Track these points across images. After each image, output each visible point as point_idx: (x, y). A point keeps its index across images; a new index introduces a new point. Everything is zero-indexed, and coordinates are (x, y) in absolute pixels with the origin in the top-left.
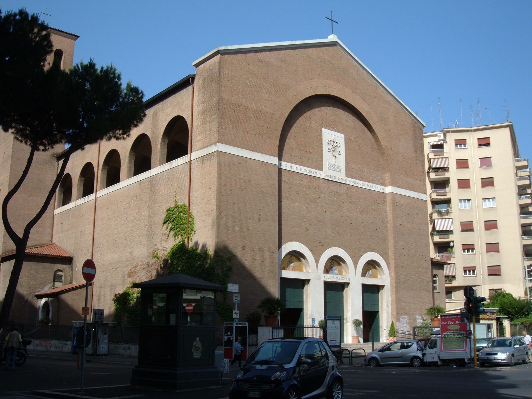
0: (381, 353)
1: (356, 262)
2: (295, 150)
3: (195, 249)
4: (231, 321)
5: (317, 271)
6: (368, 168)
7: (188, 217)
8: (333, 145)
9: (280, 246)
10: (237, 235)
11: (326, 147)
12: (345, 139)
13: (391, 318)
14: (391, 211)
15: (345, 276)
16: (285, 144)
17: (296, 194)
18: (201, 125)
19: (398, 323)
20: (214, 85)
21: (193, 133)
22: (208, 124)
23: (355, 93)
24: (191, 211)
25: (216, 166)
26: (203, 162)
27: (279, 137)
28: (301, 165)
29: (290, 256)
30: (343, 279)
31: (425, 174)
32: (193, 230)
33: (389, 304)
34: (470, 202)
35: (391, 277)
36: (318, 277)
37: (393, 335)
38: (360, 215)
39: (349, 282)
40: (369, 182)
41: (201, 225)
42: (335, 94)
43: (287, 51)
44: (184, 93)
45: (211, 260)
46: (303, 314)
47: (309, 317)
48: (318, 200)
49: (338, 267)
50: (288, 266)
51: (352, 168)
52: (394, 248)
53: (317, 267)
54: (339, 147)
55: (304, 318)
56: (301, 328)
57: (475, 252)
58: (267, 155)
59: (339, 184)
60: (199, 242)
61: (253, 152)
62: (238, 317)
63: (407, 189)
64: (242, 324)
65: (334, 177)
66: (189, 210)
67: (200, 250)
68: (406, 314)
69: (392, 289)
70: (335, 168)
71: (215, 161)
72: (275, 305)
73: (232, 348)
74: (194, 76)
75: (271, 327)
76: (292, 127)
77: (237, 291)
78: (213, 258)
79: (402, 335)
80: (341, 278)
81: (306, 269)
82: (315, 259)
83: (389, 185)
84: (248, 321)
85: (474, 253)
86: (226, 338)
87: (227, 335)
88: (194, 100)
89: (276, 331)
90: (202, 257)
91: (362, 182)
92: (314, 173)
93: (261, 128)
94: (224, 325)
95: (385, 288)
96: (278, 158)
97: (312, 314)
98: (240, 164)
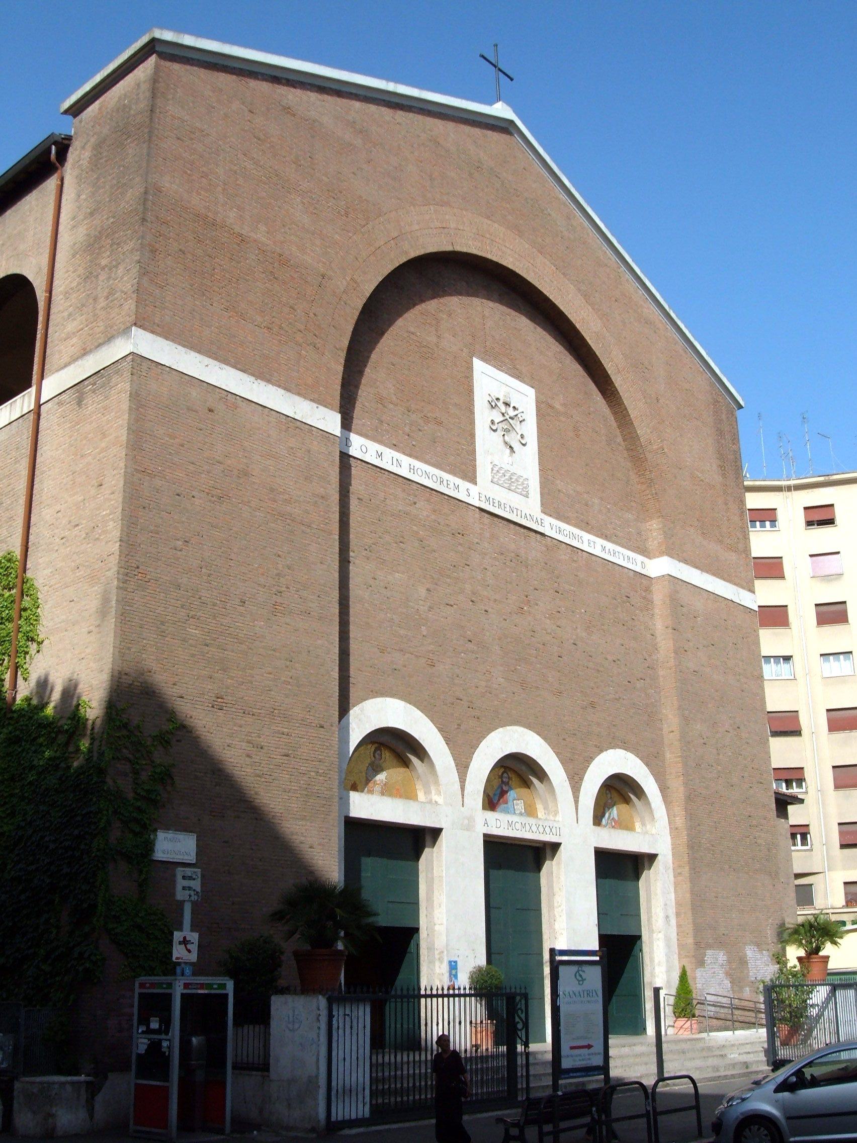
0: (786, 1094)
1: (576, 778)
2: (391, 406)
3: (36, 707)
4: (165, 975)
5: (463, 801)
6: (601, 499)
7: (19, 594)
8: (504, 411)
9: (344, 710)
10: (193, 655)
11: (483, 416)
12: (538, 403)
13: (676, 956)
14: (670, 630)
15: (546, 819)
16: (363, 381)
17: (395, 545)
18: (79, 284)
19: (699, 973)
20: (130, 151)
21: (51, 317)
22: (103, 276)
23: (563, 274)
24: (29, 574)
25: (125, 406)
26: (79, 403)
27: (345, 352)
28: (410, 455)
29: (373, 750)
30: (541, 829)
31: (747, 537)
32: (33, 640)
33: (672, 911)
34: (791, 662)
35: (674, 830)
36: (466, 822)
37: (688, 1011)
38: (584, 634)
39: (559, 842)
40: (606, 538)
41: (64, 617)
42: (508, 262)
43: (373, 108)
44: (31, 203)
45: (93, 739)
46: (418, 946)
47: (437, 956)
48: (463, 571)
49: (524, 791)
50: (368, 781)
51: (559, 491)
52: (680, 740)
53: (463, 788)
54: (521, 422)
55: (422, 958)
56: (408, 997)
57: (806, 788)
58: (305, 398)
59: (522, 530)
60: (51, 679)
61: (259, 380)
62: (193, 957)
63: (707, 572)
64: (209, 986)
65: (508, 509)
66: (25, 570)
67: (55, 707)
68: (720, 943)
69: (680, 866)
70: (512, 482)
71: (122, 388)
72: (338, 910)
73: (166, 1084)
74: (66, 142)
75: (324, 995)
76: (383, 334)
77: (191, 858)
78: (103, 733)
79: (713, 1009)
80: (534, 828)
81: (427, 792)
82: (454, 760)
83: (662, 554)
84: (232, 974)
85: (804, 790)
86: (142, 1044)
87: (149, 1031)
88: (62, 215)
89: (341, 1012)
90: (60, 732)
91: (586, 536)
92: (452, 485)
93: (286, 310)
94: (137, 991)
95: (659, 864)
96: (339, 416)
97: (447, 945)
98: (210, 410)
